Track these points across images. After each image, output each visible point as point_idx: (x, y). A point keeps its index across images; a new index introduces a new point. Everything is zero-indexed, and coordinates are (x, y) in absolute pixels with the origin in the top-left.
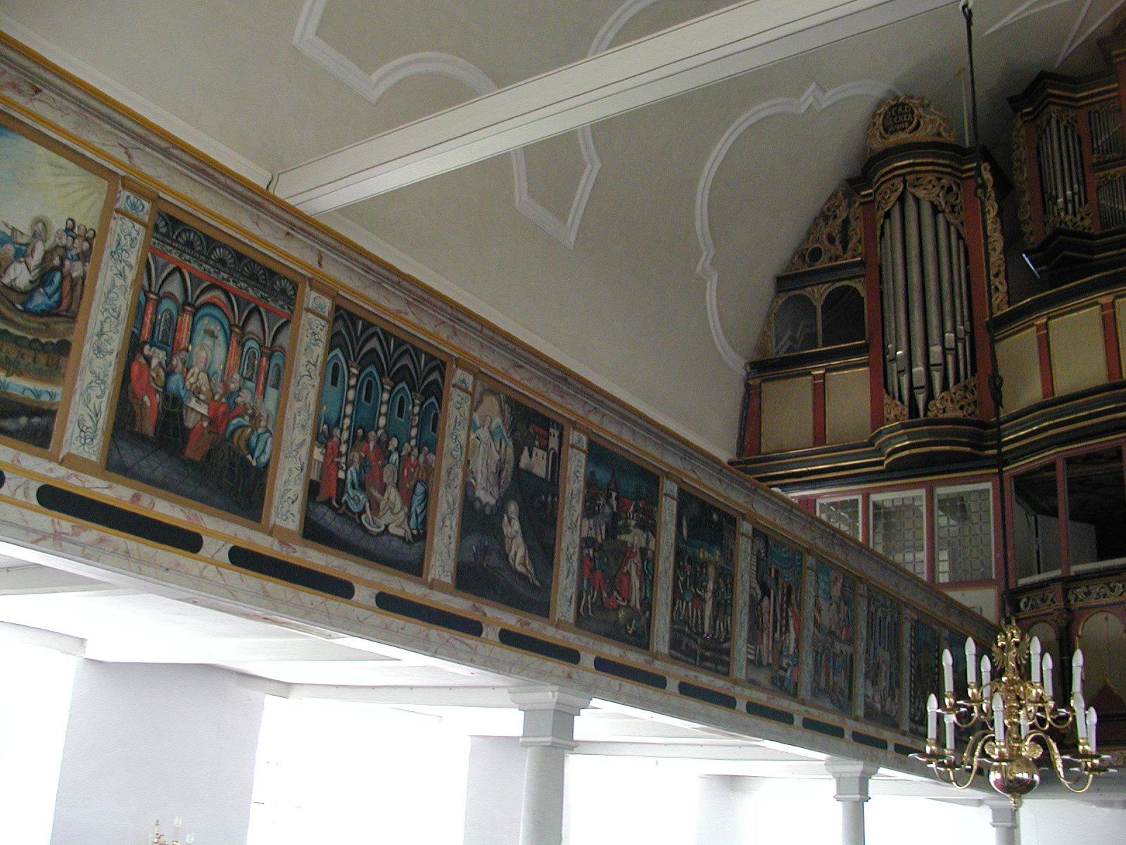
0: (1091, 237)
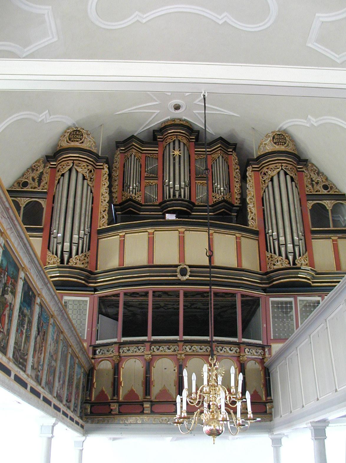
0: (141, 205)
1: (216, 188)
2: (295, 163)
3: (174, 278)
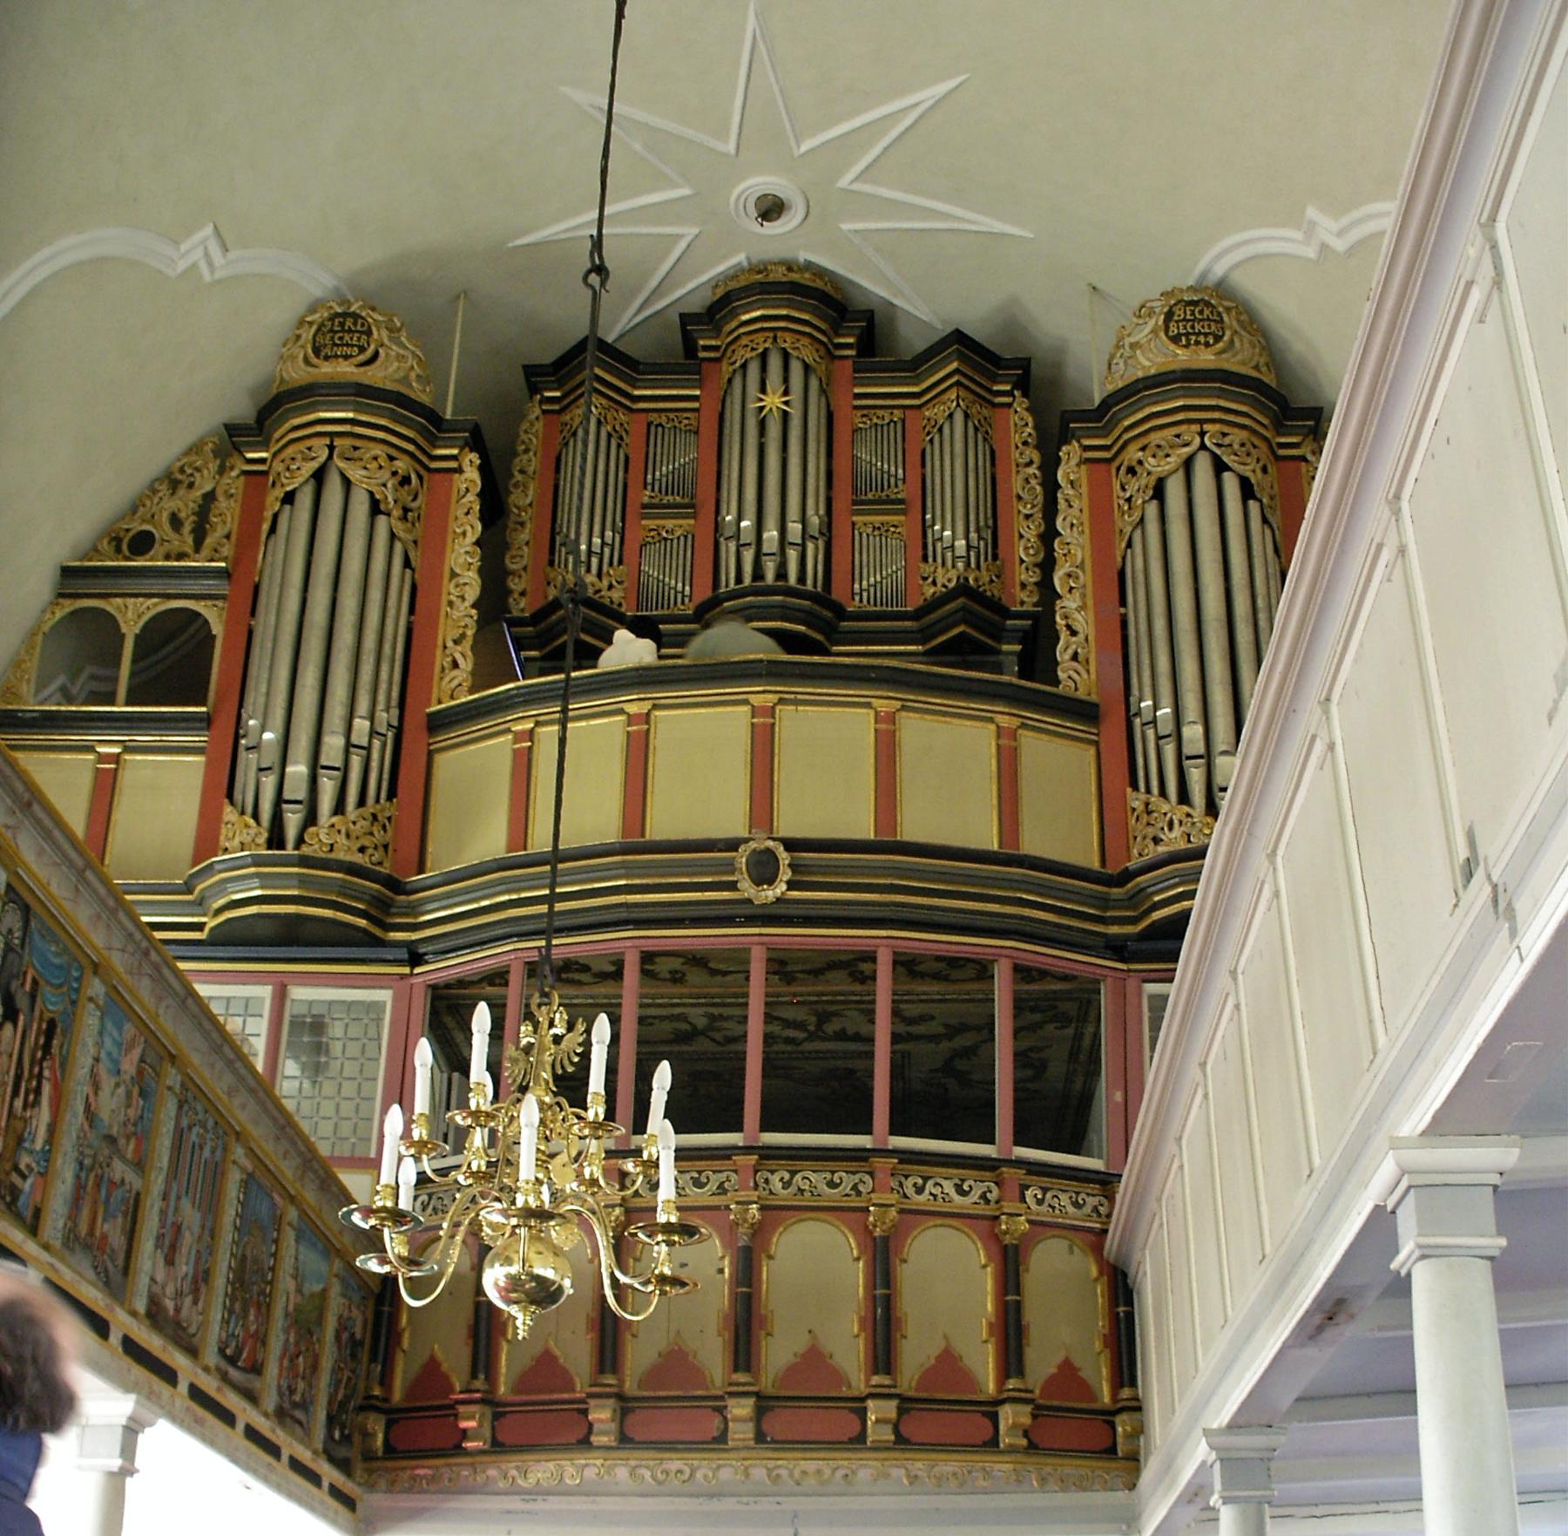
1: (939, 545)
2: (1266, 421)
3: (726, 895)
